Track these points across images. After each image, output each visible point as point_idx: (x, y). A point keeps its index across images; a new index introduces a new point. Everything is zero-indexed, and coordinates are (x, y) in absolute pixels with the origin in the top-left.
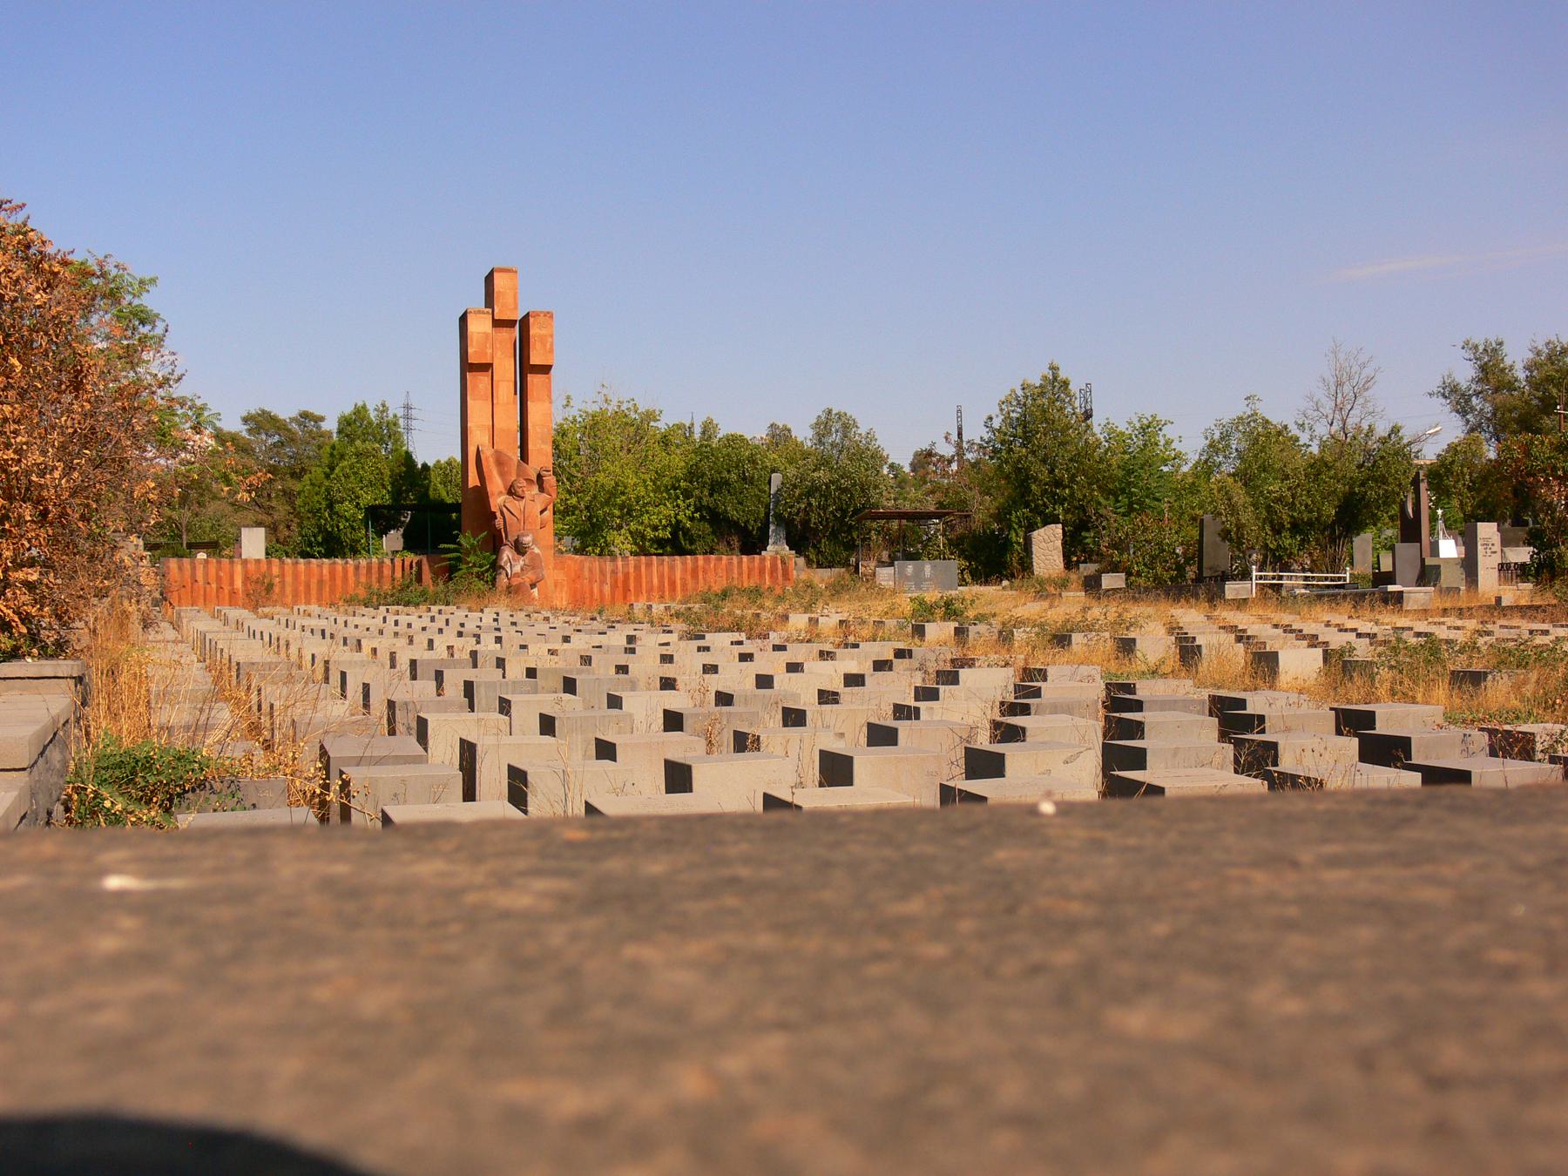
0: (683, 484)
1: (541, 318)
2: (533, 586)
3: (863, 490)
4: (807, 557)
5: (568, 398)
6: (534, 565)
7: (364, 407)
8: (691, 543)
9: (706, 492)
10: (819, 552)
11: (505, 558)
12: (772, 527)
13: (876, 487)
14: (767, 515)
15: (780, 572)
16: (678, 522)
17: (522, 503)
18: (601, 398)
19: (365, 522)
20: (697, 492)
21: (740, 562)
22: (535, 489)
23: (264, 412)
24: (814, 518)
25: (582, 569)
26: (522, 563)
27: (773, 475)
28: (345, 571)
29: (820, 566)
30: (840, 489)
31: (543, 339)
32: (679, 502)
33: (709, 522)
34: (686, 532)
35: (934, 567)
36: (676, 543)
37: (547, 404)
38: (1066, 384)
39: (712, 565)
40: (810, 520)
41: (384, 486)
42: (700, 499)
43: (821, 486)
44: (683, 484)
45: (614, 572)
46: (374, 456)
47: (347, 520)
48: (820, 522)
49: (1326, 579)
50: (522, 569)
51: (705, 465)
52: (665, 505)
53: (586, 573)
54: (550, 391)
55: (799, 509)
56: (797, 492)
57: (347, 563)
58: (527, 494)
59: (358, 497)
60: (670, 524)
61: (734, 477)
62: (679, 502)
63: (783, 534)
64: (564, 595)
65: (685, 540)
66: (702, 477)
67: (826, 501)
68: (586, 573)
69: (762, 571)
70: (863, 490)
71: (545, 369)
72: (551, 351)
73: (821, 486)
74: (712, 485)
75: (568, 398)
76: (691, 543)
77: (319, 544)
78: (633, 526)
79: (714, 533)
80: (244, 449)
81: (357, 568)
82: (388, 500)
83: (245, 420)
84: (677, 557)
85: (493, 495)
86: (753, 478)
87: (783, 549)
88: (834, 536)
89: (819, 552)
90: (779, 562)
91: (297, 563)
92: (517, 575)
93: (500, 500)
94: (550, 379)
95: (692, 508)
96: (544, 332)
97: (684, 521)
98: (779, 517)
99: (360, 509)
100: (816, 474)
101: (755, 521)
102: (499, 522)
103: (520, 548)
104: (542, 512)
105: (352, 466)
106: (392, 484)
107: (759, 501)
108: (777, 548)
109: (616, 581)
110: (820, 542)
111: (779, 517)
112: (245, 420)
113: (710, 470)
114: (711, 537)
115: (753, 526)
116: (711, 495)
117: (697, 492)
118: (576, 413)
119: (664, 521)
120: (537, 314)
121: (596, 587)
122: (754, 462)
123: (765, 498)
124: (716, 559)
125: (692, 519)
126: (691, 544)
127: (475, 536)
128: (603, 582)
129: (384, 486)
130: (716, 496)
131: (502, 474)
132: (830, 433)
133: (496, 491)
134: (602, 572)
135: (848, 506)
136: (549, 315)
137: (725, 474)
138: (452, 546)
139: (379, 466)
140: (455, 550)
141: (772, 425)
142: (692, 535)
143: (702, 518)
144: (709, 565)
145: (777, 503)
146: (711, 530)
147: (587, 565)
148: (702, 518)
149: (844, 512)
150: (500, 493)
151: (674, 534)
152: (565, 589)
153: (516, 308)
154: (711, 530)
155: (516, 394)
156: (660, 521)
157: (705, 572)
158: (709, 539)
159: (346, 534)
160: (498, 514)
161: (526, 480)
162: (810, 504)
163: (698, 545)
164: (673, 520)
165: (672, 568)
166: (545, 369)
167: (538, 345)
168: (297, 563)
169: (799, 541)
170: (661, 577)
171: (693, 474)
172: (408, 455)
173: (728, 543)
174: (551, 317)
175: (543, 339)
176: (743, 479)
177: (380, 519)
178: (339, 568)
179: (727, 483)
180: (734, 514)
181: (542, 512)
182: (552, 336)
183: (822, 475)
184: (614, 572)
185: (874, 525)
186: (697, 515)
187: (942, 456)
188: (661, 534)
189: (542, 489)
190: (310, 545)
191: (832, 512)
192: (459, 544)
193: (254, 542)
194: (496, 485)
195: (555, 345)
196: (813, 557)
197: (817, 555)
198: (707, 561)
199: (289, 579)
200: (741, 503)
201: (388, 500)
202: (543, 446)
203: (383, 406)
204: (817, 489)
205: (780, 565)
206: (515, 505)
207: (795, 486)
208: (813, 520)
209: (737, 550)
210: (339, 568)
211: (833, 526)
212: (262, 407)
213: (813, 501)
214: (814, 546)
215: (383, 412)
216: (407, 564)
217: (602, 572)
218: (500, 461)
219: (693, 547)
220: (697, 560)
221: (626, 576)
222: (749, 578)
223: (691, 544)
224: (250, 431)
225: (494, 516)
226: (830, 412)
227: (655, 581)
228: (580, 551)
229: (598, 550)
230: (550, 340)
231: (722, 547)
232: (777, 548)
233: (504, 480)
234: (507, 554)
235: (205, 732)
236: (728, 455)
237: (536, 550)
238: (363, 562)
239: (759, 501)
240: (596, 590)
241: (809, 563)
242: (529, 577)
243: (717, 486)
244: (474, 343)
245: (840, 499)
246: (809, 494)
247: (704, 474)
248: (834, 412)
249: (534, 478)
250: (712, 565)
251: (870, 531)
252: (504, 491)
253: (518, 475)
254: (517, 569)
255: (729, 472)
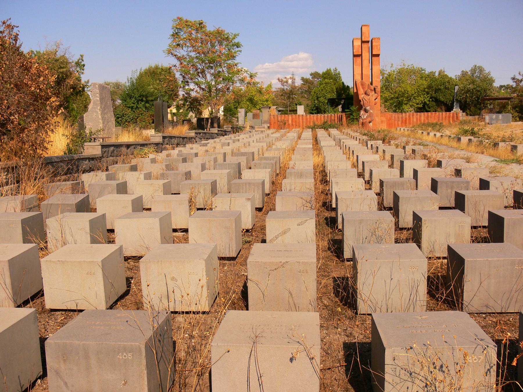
0: (426, 90)
1: (376, 40)
2: (370, 122)
3: (485, 91)
4: (466, 113)
5: (392, 64)
6: (371, 115)
7: (330, 69)
8: (429, 108)
9: (433, 93)
10: (471, 111)
11: (361, 114)
12: (455, 103)
13: (490, 90)
14: (453, 99)
15: (455, 117)
16: (425, 102)
17: (369, 97)
18: (402, 64)
19: (327, 103)
20: (431, 93)
21: (442, 114)
22: (373, 92)
23: (316, 72)
24: (468, 100)
25: (392, 116)
26: (367, 115)
27: (456, 87)
28: (321, 118)
29: (471, 115)
30: (477, 91)
31: (377, 46)
32: (425, 96)
33: (435, 102)
34: (428, 105)
35: (502, 116)
36: (423, 109)
37: (378, 66)
38: (39, 52)
39: (433, 115)
40: (467, 101)
41: (334, 93)
42: (432, 95)
43: (470, 90)
44: (426, 90)
45: (402, 118)
46: (330, 84)
47: (322, 103)
48: (471, 102)
49: (303, 122)
50: (367, 117)
51: (433, 84)
52: (421, 97)
53: (393, 118)
54: (379, 62)
55: (463, 97)
56: (463, 92)
57: (321, 115)
58: (371, 94)
59: (326, 96)
60: (422, 103)
61: (442, 87)
62: (425, 96)
63: (458, 105)
64: (385, 125)
65: (427, 107)
66: (432, 88)
67: (472, 94)
68: (393, 118)
69: (449, 117)
70: (485, 91)
71: (378, 55)
72: (379, 50)
73: (470, 90)
74: (436, 90)
75: (392, 64)
76: (429, 108)
77: (315, 110)
78: (411, 104)
79: (436, 105)
80: (311, 83)
81: (324, 117)
82: (335, 96)
83: (311, 75)
84: (422, 113)
85: (360, 94)
86: (449, 87)
87: (458, 110)
88: (475, 106)
89: (471, 111)
90: (455, 114)
91: (307, 116)
92: (365, 119)
93: (362, 96)
94: (379, 58)
95: (429, 98)
96: (377, 44)
97: (427, 102)
98: (457, 100)
99: (326, 99)
100: (469, 86)
101: (449, 101)
102: (362, 103)
103: (366, 111)
104: (375, 100)
105: (324, 87)
106: (337, 92)
107: (451, 95)
108: (456, 109)
109: (403, 121)
110: (471, 108)
111: (457, 100)
112: (311, 75)
113: (435, 85)
114: (435, 106)
115: (449, 103)
116: (435, 93)
117: (431, 93)
118: (395, 69)
119: (420, 102)
120: (375, 39)
121: (396, 122)
122: (449, 83)
123: (453, 94)
124: (435, 113)
125: (429, 101)
126: (429, 109)
127: (355, 107)
128: (398, 121)
129: (334, 93)
130: (436, 94)
131: (363, 88)
132: (476, 73)
133: (361, 93)
134: (398, 117)
135: (480, 96)
136: (379, 39)
137: (440, 87)
138: (348, 110)
139: (332, 86)
140: (349, 112)
141: (462, 71)
142: (429, 106)
143: (432, 101)
144: (432, 115)
145: (457, 95)
146: (435, 104)
147: (393, 115)
148: (432, 101)
149: (478, 98)
150: (362, 94)
151: (424, 106)
152: (385, 123)
153: (369, 37)
154: (435, 104)
155: (369, 63)
156: (419, 102)
157: (431, 117)
158: (435, 107)
159: (322, 107)
160: (362, 100)
161: (370, 90)
162: (467, 96)
163: (432, 109)
164: (423, 101)
165: (420, 116)
166: (378, 55)
167: (375, 48)
168: (307, 116)
169: (464, 107)
170: (417, 119)
171: (430, 87)
172: (343, 83)
173: (441, 108)
174: (379, 39)
175: (377, 46)
176: (445, 88)
177: (333, 103)
178: (319, 117)
179: (440, 89)
180: (442, 99)
181: (375, 100)
182: (380, 45)
183: (471, 87)
184: (402, 118)
185: (489, 102)
186: (431, 100)
187: (518, 79)
188: (419, 106)
189: (375, 93)
190: (313, 110)
191: (474, 98)
192: (350, 109)
193: (301, 110)
194: (361, 91)
195: (383, 49)
196: (468, 113)
197: (470, 112)
198: (432, 114)
199: (305, 120)
200: (444, 96)
201: (335, 96)
202: (377, 79)
203: (336, 69)
204: (469, 91)
205: (455, 115)
206: (367, 98)
207: (462, 90)
208: (468, 101)
209: (444, 110)
210: (319, 117)
211: (475, 103)
212: (340, 72)
213: (468, 95)
214: (469, 109)
215: (335, 70)
216: (338, 115)
217: (398, 117)
218: (363, 85)
219: (430, 110)
220: (428, 114)
221: (406, 119)
222: (445, 120)
223: (429, 109)
224: (312, 78)
225: (360, 101)
226: (476, 66)
227: (415, 120)
228: (395, 111)
229: (400, 111)
230: (379, 46)
231: (439, 109)
232: (456, 109)
233: (364, 90)
234: (362, 112)
235: (54, 162)
236: (441, 81)
237: (371, 111)
238: (326, 115)
239: (451, 95)
240: (396, 123)
241: (467, 115)
242: (368, 120)
243: (437, 90)
244: (356, 48)
245: (477, 94)
246: (467, 92)
247: (433, 87)
248: (477, 66)
249: (373, 89)
250: (433, 115)
251: (487, 104)
252: (363, 93)
253: (368, 88)
254: (365, 117)
255: (441, 86)
